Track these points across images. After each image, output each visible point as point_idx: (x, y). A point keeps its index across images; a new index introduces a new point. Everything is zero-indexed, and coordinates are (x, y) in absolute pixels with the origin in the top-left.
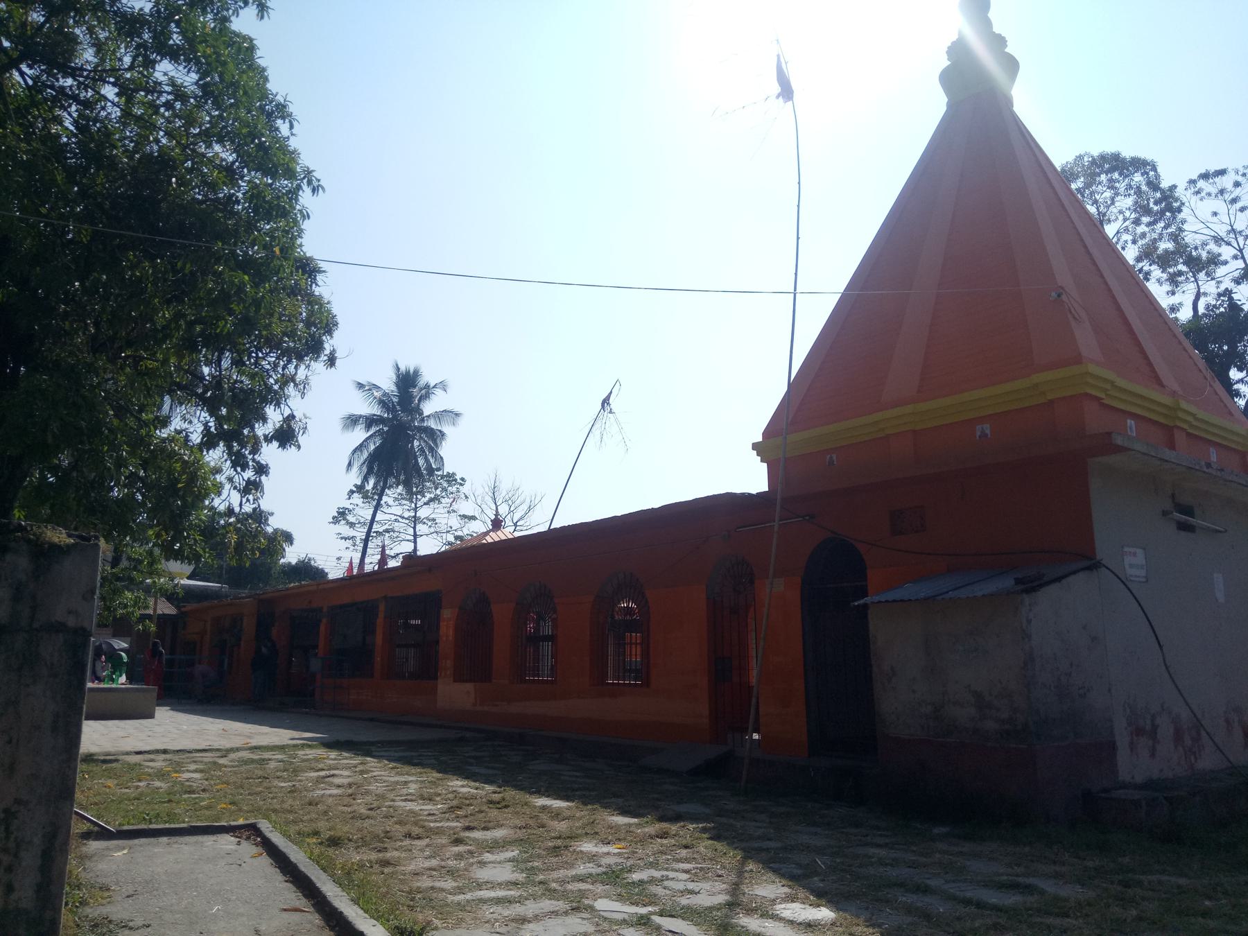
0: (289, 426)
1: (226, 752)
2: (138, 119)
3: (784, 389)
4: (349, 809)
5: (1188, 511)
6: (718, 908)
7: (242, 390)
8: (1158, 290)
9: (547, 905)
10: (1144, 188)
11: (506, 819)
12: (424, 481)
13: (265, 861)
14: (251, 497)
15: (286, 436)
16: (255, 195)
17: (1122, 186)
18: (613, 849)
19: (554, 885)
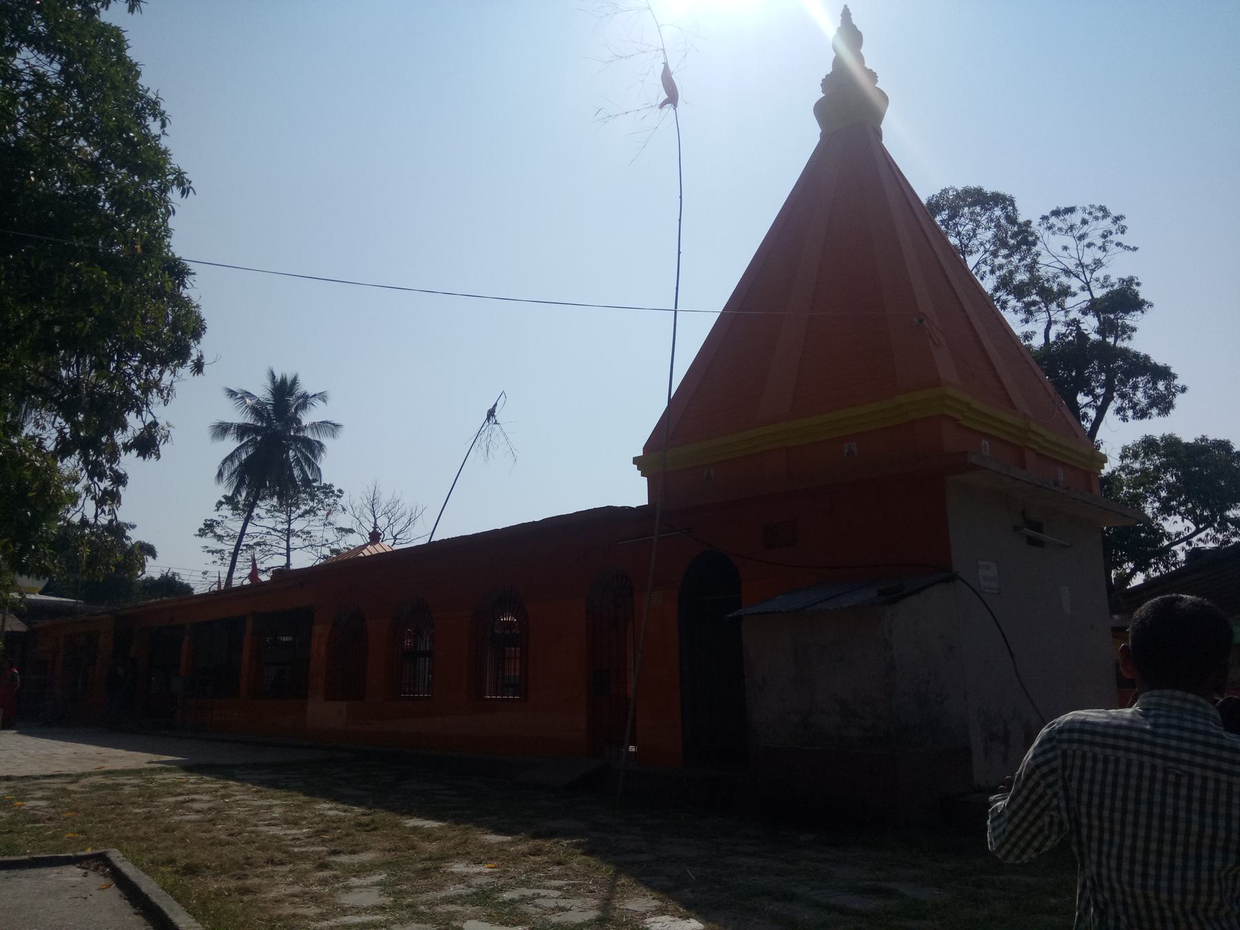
1: (77, 778)
4: (208, 836)
5: (1038, 527)
7: (100, 394)
8: (1013, 319)
10: (1003, 221)
12: (299, 492)
13: (114, 893)
15: (147, 444)
18: (485, 869)
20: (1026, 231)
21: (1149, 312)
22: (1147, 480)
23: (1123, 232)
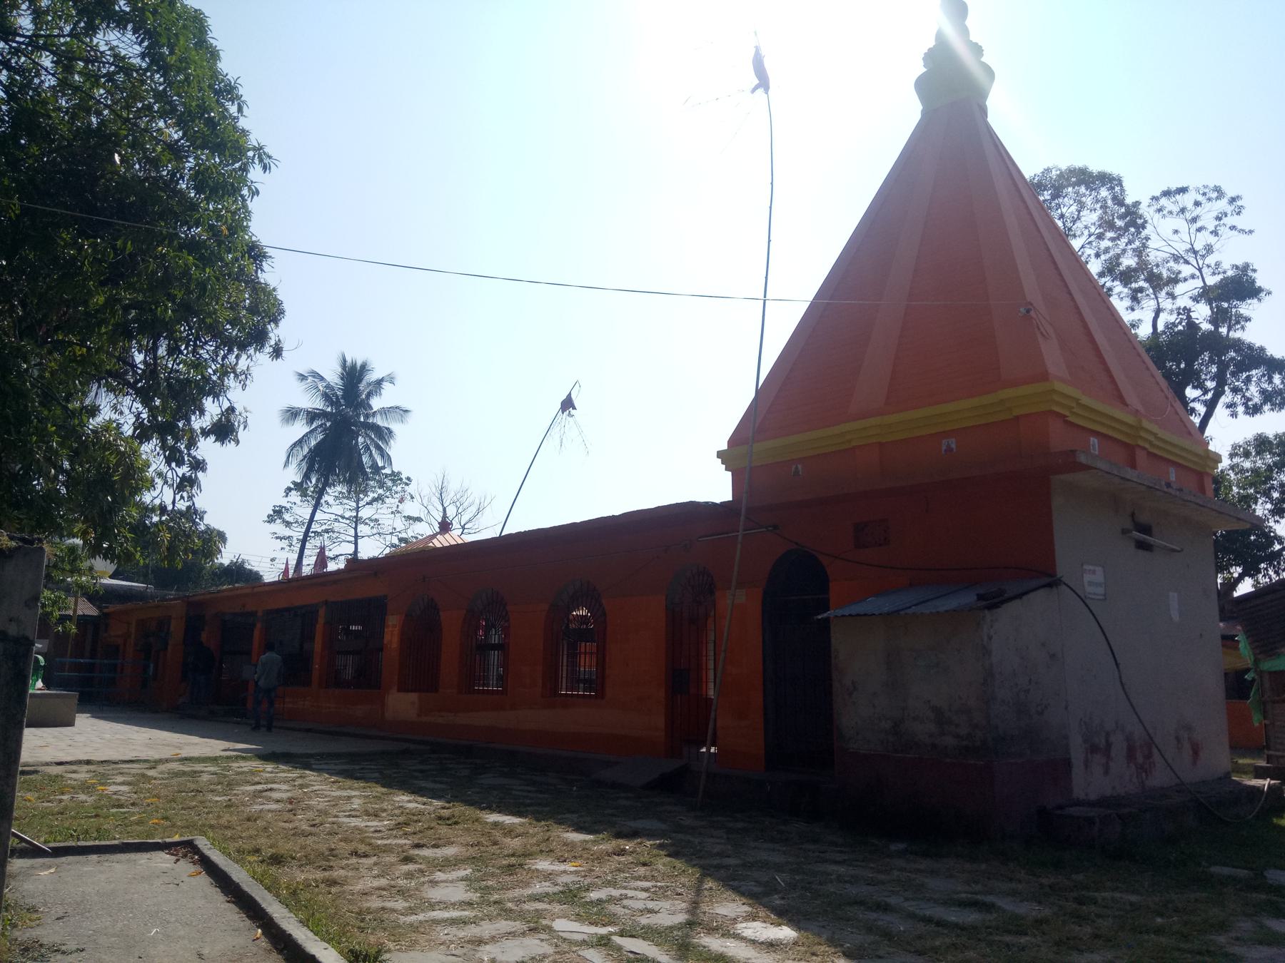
0: (228, 420)
1: (154, 764)
2: (77, 89)
3: (751, 395)
4: (291, 826)
5: (1146, 529)
6: (680, 927)
7: (178, 380)
8: (1120, 304)
9: (504, 925)
10: (1110, 203)
11: (457, 836)
12: (368, 479)
13: (204, 881)
14: (185, 494)
15: (224, 430)
16: (201, 179)
17: (1088, 201)
18: (569, 867)
19: (510, 905)
20: (1135, 213)
21: (1267, 300)
22: (1260, 480)
23: (1238, 213)
